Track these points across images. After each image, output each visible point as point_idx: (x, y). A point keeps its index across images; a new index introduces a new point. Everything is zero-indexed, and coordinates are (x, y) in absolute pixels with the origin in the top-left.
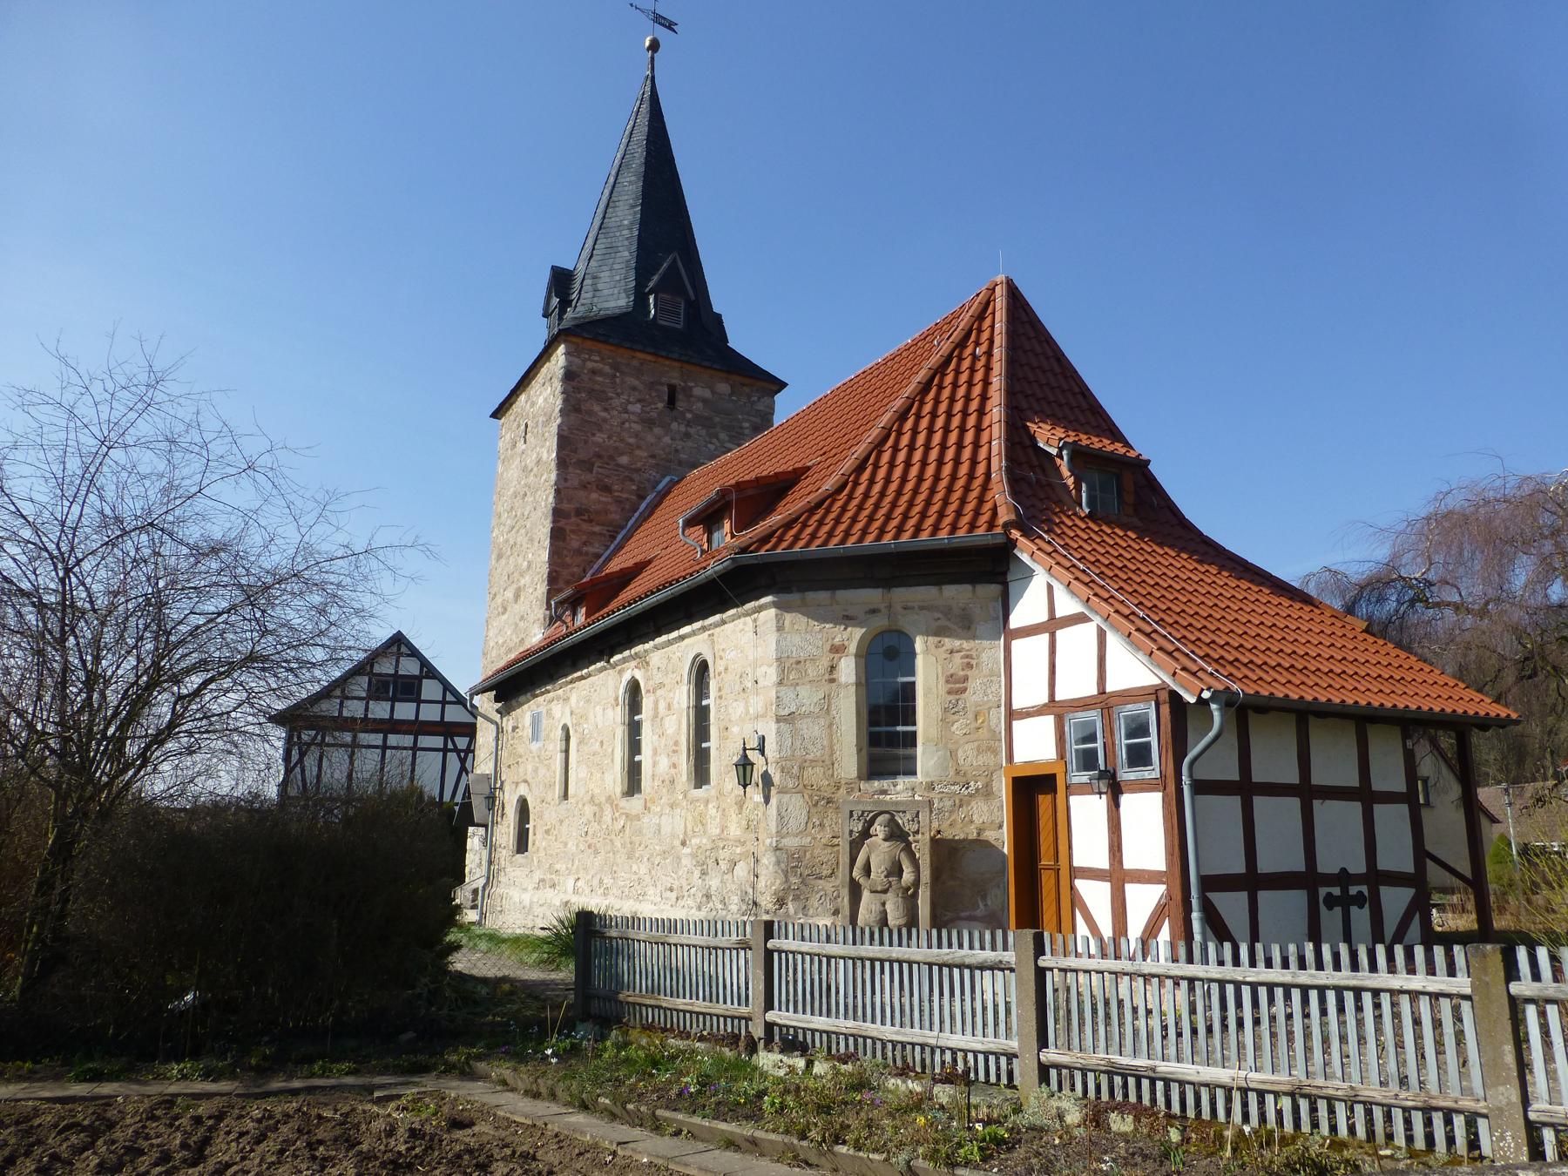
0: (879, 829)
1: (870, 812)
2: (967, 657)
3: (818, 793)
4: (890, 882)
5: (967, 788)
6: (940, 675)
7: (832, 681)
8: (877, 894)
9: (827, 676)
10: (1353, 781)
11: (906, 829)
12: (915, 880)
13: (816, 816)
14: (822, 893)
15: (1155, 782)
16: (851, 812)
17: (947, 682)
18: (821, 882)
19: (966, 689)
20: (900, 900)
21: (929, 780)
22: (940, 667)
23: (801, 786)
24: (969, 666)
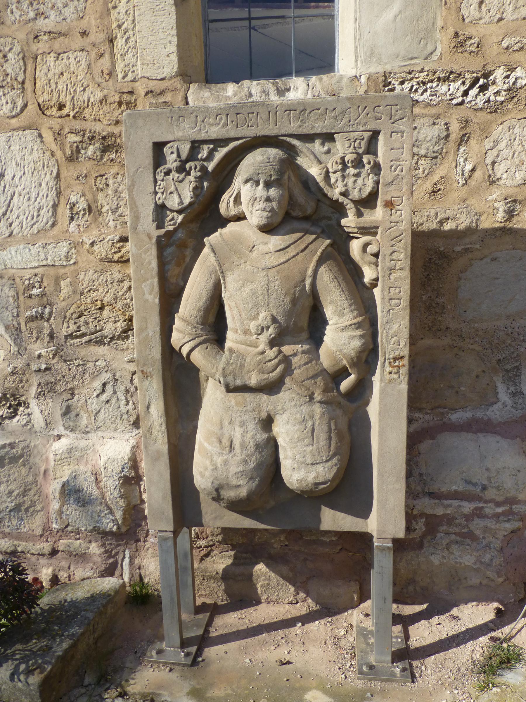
1: (219, 143)
3: (78, 125)
4: (286, 360)
5: (484, 88)
8: (248, 397)
11: (335, 193)
12: (361, 351)
13: (78, 188)
14: (106, 377)
18: (102, 350)
20: (318, 410)
21: (376, 69)
23: (32, 108)
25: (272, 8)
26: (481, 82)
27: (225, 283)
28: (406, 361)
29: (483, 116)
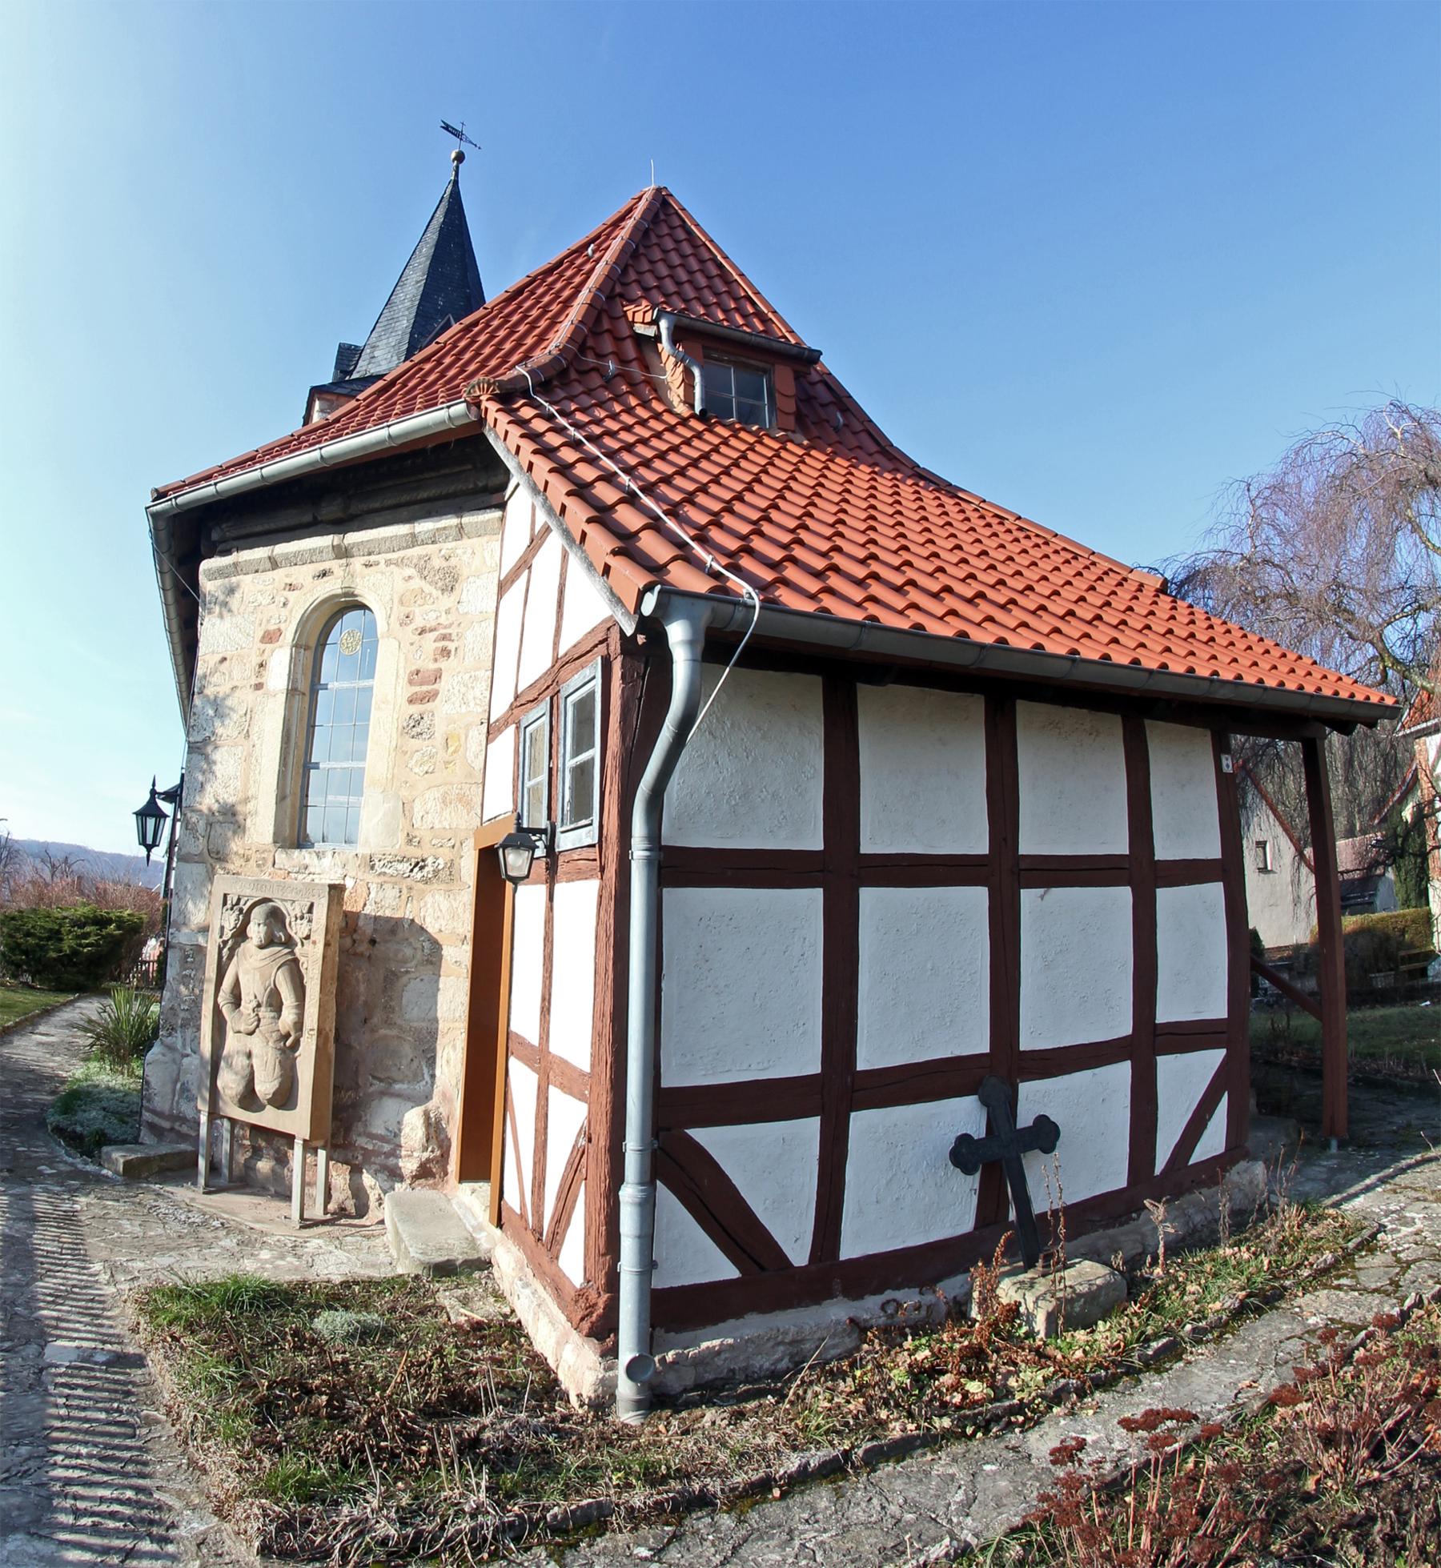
0: (256, 931)
2: (444, 637)
5: (422, 868)
6: (401, 672)
7: (259, 686)
9: (254, 681)
10: (977, 843)
15: (587, 853)
16: (225, 896)
17: (411, 682)
19: (436, 694)
22: (402, 657)
24: (445, 653)
25: (436, 424)
26: (421, 864)
27: (630, 210)
28: (315, 1032)
29: (421, 885)
